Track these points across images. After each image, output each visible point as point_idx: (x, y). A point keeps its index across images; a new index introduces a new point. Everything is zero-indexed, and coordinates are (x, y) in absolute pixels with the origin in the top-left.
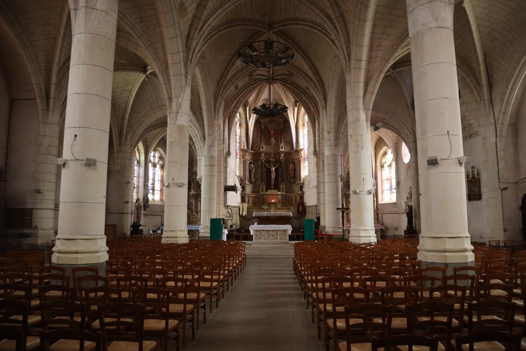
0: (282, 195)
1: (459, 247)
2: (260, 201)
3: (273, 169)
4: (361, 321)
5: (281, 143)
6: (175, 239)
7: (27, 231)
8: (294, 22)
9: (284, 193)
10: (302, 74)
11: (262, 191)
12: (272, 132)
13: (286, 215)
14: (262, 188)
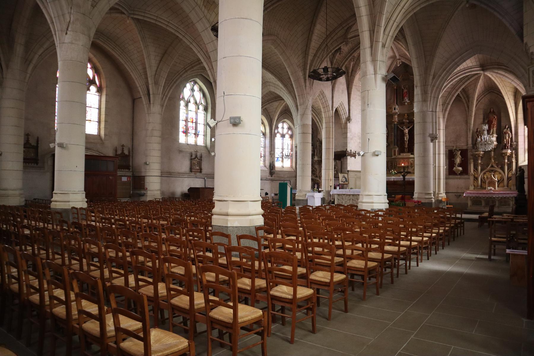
2: (392, 165)
3: (406, 131)
7: (143, 192)
11: (395, 155)
12: (405, 91)
14: (395, 151)
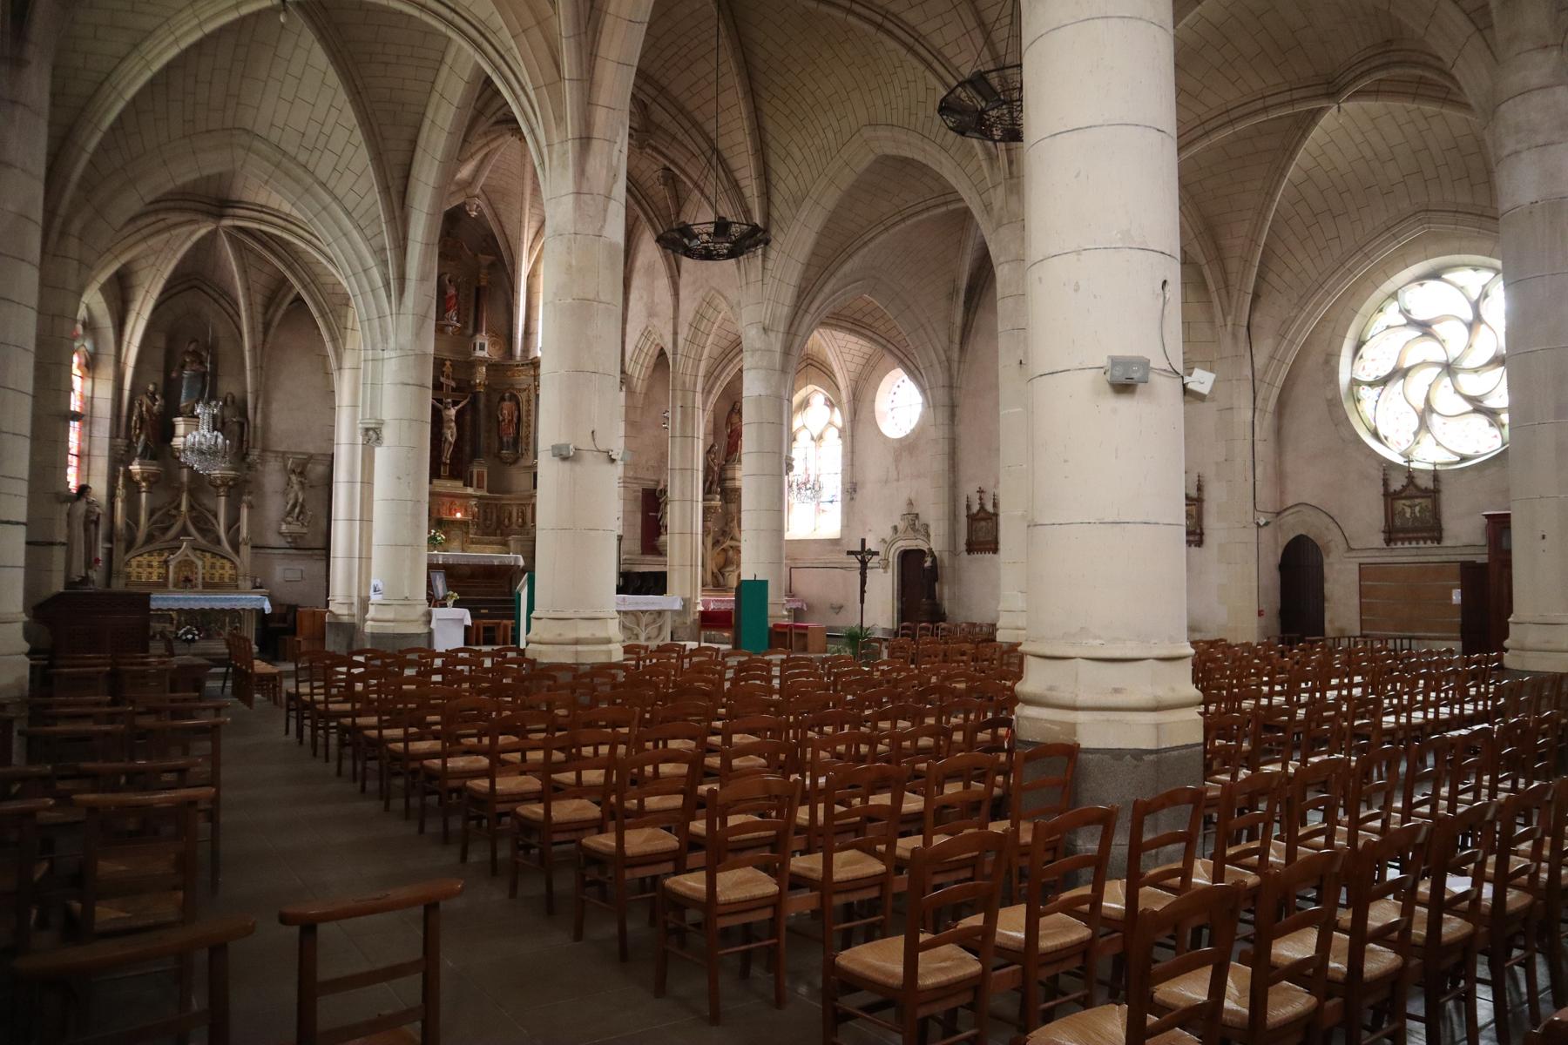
0: (479, 498)
1: (601, 634)
3: (453, 412)
4: (1344, 889)
5: (477, 330)
6: (603, 647)
10: (699, 139)
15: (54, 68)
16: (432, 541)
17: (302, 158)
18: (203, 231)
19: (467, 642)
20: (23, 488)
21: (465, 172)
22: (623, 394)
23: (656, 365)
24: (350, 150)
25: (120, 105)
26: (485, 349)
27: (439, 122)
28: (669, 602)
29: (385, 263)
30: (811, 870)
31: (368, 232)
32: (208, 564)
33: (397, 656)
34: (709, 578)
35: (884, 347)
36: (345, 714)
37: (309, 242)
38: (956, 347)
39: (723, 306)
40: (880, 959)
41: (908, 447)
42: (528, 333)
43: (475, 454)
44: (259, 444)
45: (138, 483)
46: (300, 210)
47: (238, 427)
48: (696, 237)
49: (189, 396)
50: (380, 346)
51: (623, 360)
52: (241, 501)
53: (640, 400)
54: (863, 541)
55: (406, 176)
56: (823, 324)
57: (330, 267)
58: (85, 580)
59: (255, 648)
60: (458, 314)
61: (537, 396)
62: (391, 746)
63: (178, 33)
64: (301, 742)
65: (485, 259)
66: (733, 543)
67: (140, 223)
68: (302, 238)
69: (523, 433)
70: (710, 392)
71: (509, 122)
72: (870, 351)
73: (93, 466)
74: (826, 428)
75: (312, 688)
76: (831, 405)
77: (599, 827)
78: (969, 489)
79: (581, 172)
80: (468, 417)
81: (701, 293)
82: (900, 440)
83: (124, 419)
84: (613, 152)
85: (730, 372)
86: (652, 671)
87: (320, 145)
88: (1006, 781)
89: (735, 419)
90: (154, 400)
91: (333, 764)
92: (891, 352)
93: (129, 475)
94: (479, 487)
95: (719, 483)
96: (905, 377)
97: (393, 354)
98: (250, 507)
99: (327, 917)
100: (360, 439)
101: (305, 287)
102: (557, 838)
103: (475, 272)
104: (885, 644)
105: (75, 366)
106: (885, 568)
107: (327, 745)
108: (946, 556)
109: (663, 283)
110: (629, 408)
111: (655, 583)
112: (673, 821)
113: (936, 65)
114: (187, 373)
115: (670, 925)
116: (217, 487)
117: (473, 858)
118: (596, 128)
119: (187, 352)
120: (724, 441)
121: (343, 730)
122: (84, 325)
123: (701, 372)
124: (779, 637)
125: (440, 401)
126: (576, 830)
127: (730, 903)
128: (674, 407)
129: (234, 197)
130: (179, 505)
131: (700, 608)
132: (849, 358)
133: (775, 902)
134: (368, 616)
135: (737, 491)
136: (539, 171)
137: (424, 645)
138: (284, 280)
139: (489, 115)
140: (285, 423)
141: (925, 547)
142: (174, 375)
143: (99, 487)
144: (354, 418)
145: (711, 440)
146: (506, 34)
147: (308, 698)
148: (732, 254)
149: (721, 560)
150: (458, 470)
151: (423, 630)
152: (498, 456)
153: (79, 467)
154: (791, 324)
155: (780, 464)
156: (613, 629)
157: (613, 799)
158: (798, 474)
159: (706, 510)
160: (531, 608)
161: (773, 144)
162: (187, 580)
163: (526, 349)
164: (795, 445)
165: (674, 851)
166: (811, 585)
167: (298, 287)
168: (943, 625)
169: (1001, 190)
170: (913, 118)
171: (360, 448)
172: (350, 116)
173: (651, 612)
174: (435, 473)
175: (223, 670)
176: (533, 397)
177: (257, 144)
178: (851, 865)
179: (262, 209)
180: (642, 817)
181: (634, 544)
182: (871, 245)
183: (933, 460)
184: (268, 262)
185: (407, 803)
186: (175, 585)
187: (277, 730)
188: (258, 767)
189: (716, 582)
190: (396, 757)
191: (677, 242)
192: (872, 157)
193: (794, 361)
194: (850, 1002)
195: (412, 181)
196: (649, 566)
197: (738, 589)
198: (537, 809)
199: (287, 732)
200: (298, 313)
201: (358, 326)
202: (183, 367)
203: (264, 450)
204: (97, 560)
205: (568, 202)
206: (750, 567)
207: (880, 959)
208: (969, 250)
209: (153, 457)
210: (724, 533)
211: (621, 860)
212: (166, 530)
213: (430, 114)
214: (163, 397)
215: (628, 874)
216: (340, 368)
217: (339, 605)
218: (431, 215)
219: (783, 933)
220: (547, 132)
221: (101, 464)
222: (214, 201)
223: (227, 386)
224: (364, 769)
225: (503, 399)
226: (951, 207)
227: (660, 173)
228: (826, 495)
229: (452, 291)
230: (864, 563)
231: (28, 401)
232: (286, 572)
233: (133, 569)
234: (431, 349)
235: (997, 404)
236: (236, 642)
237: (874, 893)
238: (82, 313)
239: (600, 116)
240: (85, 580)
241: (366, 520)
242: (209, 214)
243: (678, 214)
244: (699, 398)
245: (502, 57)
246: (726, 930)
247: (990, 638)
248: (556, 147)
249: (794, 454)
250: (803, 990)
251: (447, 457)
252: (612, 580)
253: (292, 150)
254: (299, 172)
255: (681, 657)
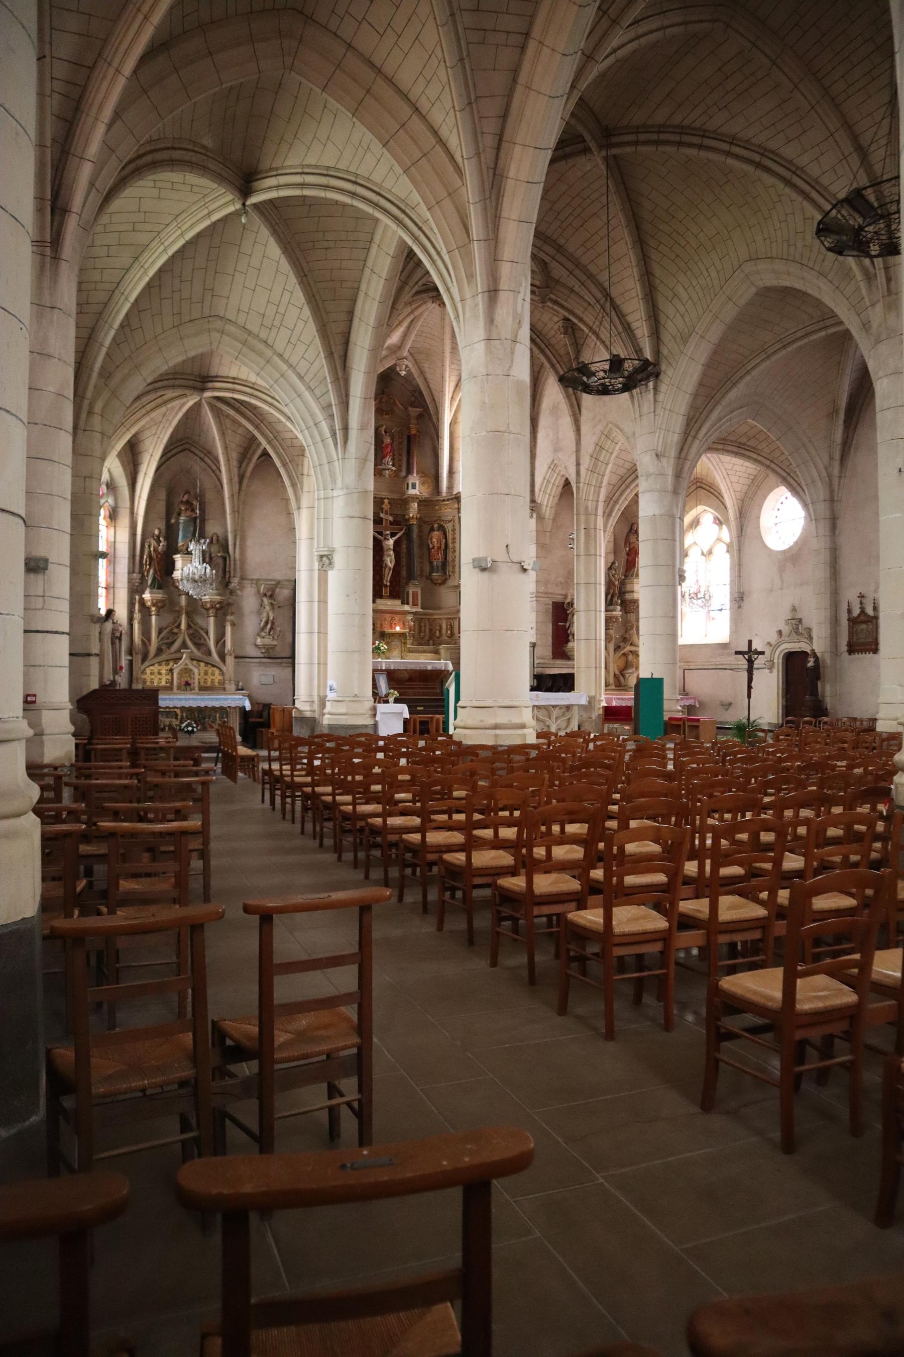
0: (415, 613)
1: (516, 720)
3: (391, 542)
5: (409, 471)
6: (519, 732)
8: (696, 140)
9: (419, 610)
13: (438, 667)
15: (80, 283)
16: (376, 651)
17: (263, 335)
18: (191, 403)
19: (405, 729)
20: (65, 606)
21: (394, 338)
22: (533, 521)
23: (562, 495)
24: (301, 324)
25: (127, 306)
26: (416, 488)
27: (371, 293)
28: (576, 697)
29: (331, 416)
30: (699, 911)
31: (318, 392)
32: (202, 672)
33: (349, 748)
34: (611, 680)
35: (768, 467)
36: (306, 785)
37: (271, 405)
38: (836, 464)
39: (620, 438)
40: (762, 985)
41: (792, 556)
42: (451, 472)
43: (410, 577)
44: (238, 575)
45: (149, 608)
46: (263, 378)
47: (221, 560)
48: (594, 374)
49: (184, 537)
50: (330, 487)
51: (532, 491)
52: (225, 621)
53: (549, 525)
54: (750, 642)
55: (347, 343)
56: (710, 449)
57: (288, 424)
58: (114, 682)
59: (239, 738)
60: (393, 459)
61: (459, 518)
62: (342, 808)
63: (166, 244)
64: (274, 809)
65: (414, 411)
66: (633, 648)
67: (145, 400)
68: (265, 401)
69: (450, 558)
70: (610, 515)
71: (431, 292)
72: (755, 473)
73: (117, 595)
74: (715, 544)
75: (281, 766)
76: (719, 522)
77: (512, 872)
78: (850, 595)
79: (490, 320)
80: (404, 546)
81: (600, 427)
82: (784, 552)
83: (138, 558)
84: (517, 303)
85: (628, 496)
86: (559, 750)
87: (277, 323)
88: (885, 847)
89: (632, 539)
90: (159, 542)
91: (298, 826)
92: (773, 470)
93: (142, 602)
94: (415, 604)
95: (619, 596)
96: (788, 494)
97: (341, 492)
98: (233, 625)
99: (281, 910)
100: (316, 565)
101: (269, 442)
102: (477, 881)
103: (405, 423)
104: (770, 734)
105: (101, 518)
106: (771, 669)
107: (293, 811)
108: (828, 662)
109: (566, 421)
110: (540, 532)
111: (566, 683)
112: (578, 869)
113: (814, 195)
114: (182, 519)
115: (572, 954)
116: (207, 609)
117: (408, 899)
118: (502, 282)
119: (182, 502)
120: (623, 558)
121: (306, 797)
122: (108, 486)
123: (602, 497)
124: (673, 726)
125: (380, 533)
126: (493, 875)
127: (624, 935)
128: (578, 529)
129: (213, 373)
130: (179, 625)
131: (604, 704)
132: (734, 479)
133: (664, 937)
134: (325, 711)
135: (636, 602)
136: (455, 324)
137: (371, 732)
138: (253, 439)
139: (414, 285)
140: (257, 557)
141: (808, 649)
142: (173, 521)
143: (121, 613)
144: (311, 546)
145: (611, 558)
146: (423, 208)
147: (278, 773)
148: (626, 388)
149: (622, 663)
150: (397, 592)
151: (369, 722)
152: (429, 578)
153: (107, 597)
154: (681, 450)
155: (674, 576)
156: (527, 716)
157: (524, 851)
158: (687, 586)
159: (608, 620)
160: (457, 699)
161: (661, 287)
162: (187, 684)
163: (450, 487)
164: (687, 560)
165: (577, 893)
166: (703, 685)
167: (264, 443)
168: (825, 719)
169: (879, 308)
170: (792, 250)
171: (316, 573)
172: (299, 296)
173: (560, 707)
174: (377, 594)
175: (215, 755)
176: (457, 527)
177: (230, 328)
178: (732, 908)
179: (234, 381)
180: (549, 866)
181: (545, 650)
182: (754, 373)
183: (815, 570)
184: (240, 425)
185: (356, 856)
186: (178, 689)
187: (254, 799)
188: (245, 839)
189: (618, 682)
190: (346, 817)
191: (577, 381)
192: (753, 290)
193: (685, 484)
194: (731, 1023)
195: (351, 346)
196: (558, 668)
197: (637, 686)
198: (461, 857)
199: (263, 801)
200: (264, 464)
201: (312, 472)
202: (179, 514)
203: (242, 578)
204: (121, 668)
205: (481, 347)
206: (648, 666)
207: (762, 985)
208: (848, 371)
209: (160, 588)
210: (625, 640)
211: (529, 898)
212: (170, 645)
213: (363, 287)
214: (166, 539)
215: (536, 911)
216: (299, 508)
217: (304, 703)
218: (367, 373)
219: (672, 967)
220: (460, 290)
221: (122, 595)
222: (197, 377)
223: (212, 528)
224: (322, 828)
225: (432, 530)
226: (831, 331)
227: (560, 324)
228: (715, 604)
229: (388, 440)
230: (751, 662)
231: (67, 538)
232: (261, 677)
233: (147, 677)
234: (371, 486)
235: (877, 514)
236: (224, 732)
237: (757, 935)
238: (105, 477)
239: (505, 269)
240: (114, 682)
241: (323, 632)
242: (194, 388)
243: (577, 358)
244: (600, 521)
245: (420, 228)
246: (621, 958)
247: (872, 729)
248: (468, 302)
249: (686, 567)
250: (690, 1018)
251: (387, 580)
252: (526, 680)
253: (255, 330)
254: (261, 346)
255: (587, 742)
